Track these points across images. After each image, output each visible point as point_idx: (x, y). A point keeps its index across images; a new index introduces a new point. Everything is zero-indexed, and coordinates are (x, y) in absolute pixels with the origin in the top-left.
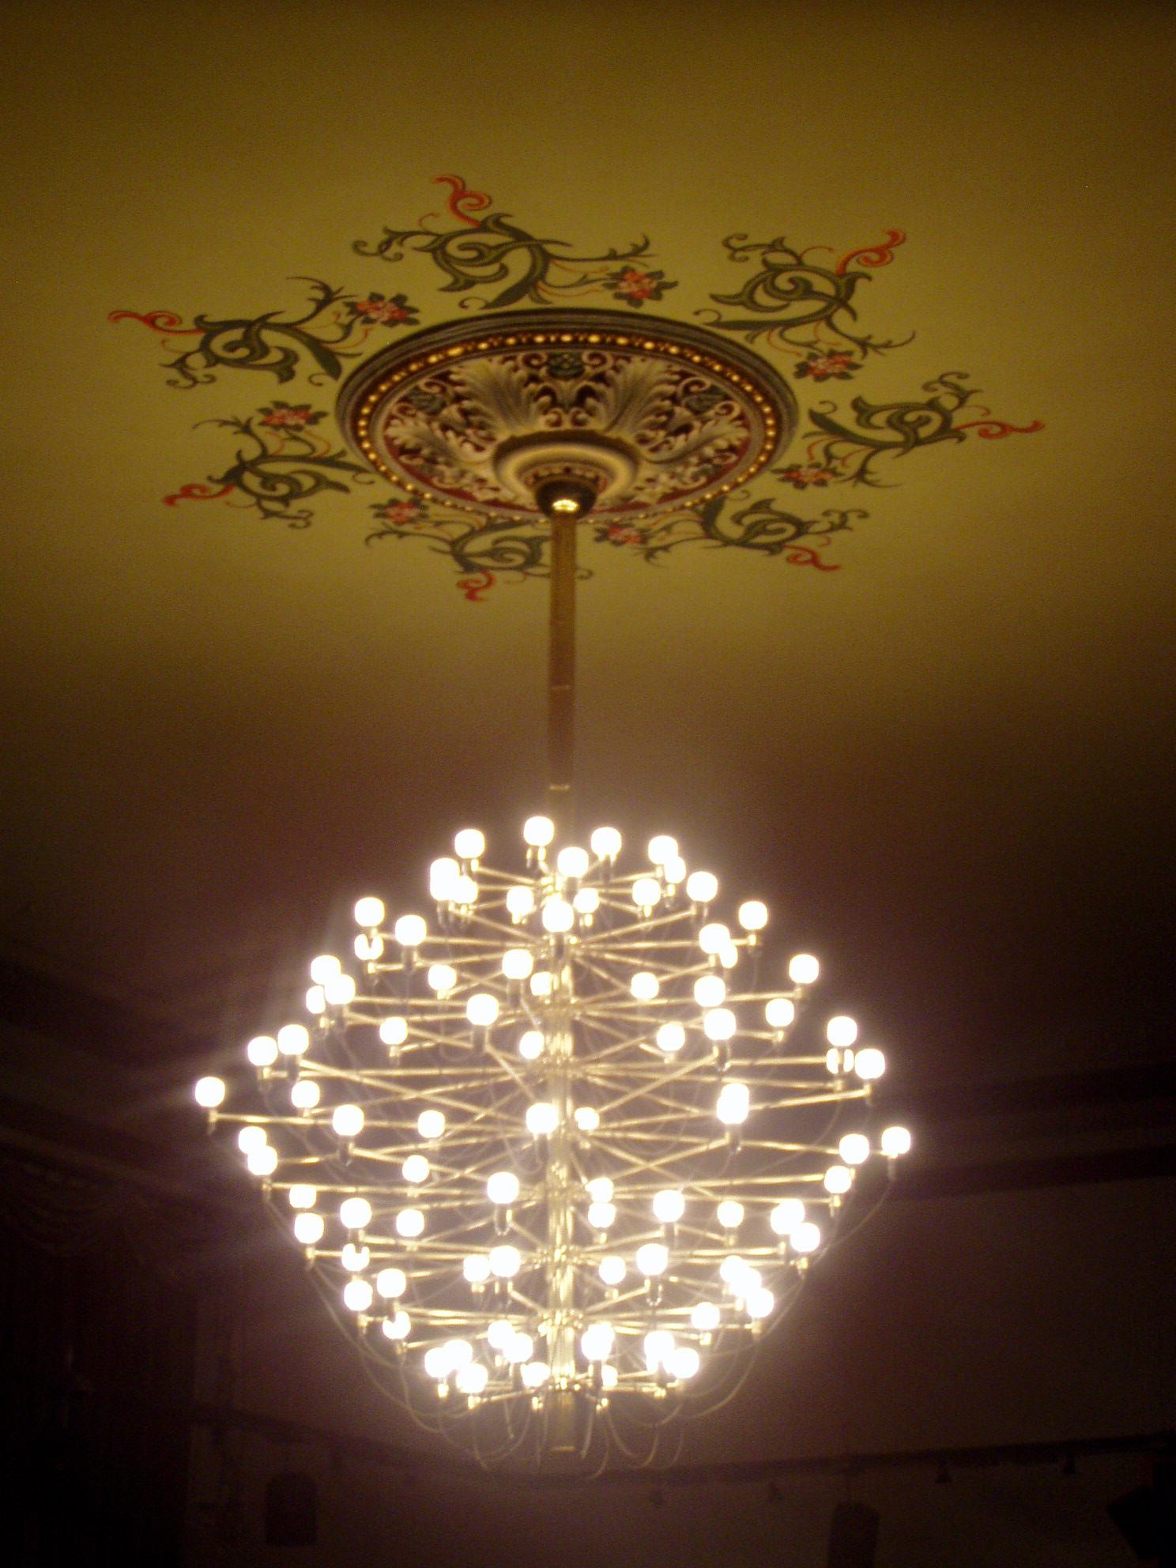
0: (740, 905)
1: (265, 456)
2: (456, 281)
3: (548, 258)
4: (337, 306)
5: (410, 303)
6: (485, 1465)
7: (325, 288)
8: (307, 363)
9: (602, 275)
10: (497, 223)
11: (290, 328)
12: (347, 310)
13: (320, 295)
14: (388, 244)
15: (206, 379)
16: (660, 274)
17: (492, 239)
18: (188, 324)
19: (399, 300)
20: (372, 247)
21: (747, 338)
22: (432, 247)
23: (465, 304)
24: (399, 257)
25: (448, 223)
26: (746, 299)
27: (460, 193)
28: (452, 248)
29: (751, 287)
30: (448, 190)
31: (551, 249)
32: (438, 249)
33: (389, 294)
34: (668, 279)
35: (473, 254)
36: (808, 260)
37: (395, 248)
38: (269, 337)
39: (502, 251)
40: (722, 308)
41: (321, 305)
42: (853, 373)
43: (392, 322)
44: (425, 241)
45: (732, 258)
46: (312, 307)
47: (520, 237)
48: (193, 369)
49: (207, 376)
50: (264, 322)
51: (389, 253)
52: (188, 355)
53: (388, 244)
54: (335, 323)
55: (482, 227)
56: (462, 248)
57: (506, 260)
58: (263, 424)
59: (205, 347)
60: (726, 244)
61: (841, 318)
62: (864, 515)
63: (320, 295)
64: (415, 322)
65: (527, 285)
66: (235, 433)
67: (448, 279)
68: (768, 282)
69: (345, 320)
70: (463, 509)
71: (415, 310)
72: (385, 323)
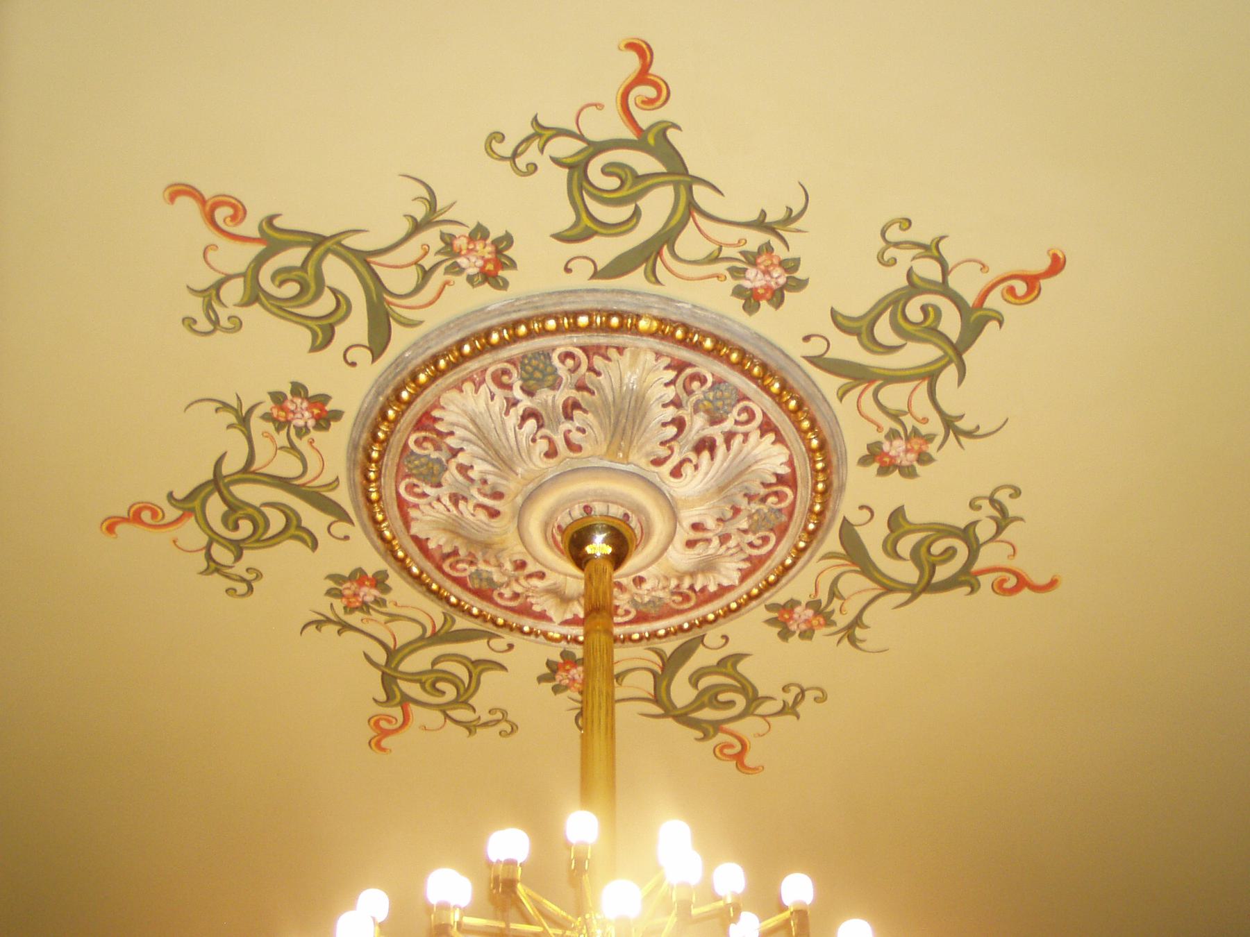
0: (852, 916)
1: (248, 473)
2: (734, 666)
3: (656, 700)
4: (842, 620)
5: (776, 630)
6: (653, 612)
7: (853, 641)
8: (873, 536)
9: (374, 615)
10: (708, 730)
11: (888, 586)
12: (834, 617)
13: (859, 632)
14: (796, 702)
15: (978, 503)
16: (556, 690)
17: (707, 714)
18: (986, 581)
19: (785, 634)
20: (809, 695)
21: (454, 621)
22: (757, 702)
23: (724, 641)
24: (785, 689)
25: (746, 727)
26: (478, 666)
27: (739, 758)
28: (741, 702)
29: (475, 681)
30: (749, 760)
31: (657, 710)
32: (754, 698)
33: (794, 639)
34: (548, 686)
35: (722, 697)
36: (437, 716)
37: (790, 698)
38: (907, 572)
39: (698, 704)
40: (321, 535)
41: (857, 621)
42: (331, 584)
43: (792, 604)
44: (766, 708)
45: (504, 713)
46: (866, 618)
47: (683, 717)
48: (992, 518)
49: (980, 508)
50: (915, 591)
51: (795, 691)
52: (992, 539)
53: (796, 702)
54: (845, 599)
55: (717, 726)
56: (731, 703)
57: (693, 693)
58: (929, 438)
59: (974, 549)
60: (514, 728)
61: (231, 466)
62: (1016, 492)
63: (859, 632)
64: (770, 608)
65: (671, 665)
66: (961, 417)
67: (742, 667)
68: (462, 690)
69: (836, 603)
70: (520, 630)
71: (771, 622)
72: (798, 603)
